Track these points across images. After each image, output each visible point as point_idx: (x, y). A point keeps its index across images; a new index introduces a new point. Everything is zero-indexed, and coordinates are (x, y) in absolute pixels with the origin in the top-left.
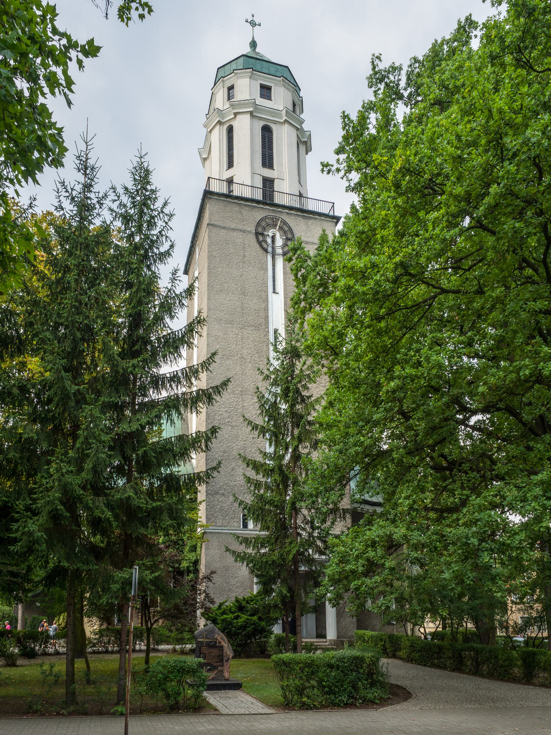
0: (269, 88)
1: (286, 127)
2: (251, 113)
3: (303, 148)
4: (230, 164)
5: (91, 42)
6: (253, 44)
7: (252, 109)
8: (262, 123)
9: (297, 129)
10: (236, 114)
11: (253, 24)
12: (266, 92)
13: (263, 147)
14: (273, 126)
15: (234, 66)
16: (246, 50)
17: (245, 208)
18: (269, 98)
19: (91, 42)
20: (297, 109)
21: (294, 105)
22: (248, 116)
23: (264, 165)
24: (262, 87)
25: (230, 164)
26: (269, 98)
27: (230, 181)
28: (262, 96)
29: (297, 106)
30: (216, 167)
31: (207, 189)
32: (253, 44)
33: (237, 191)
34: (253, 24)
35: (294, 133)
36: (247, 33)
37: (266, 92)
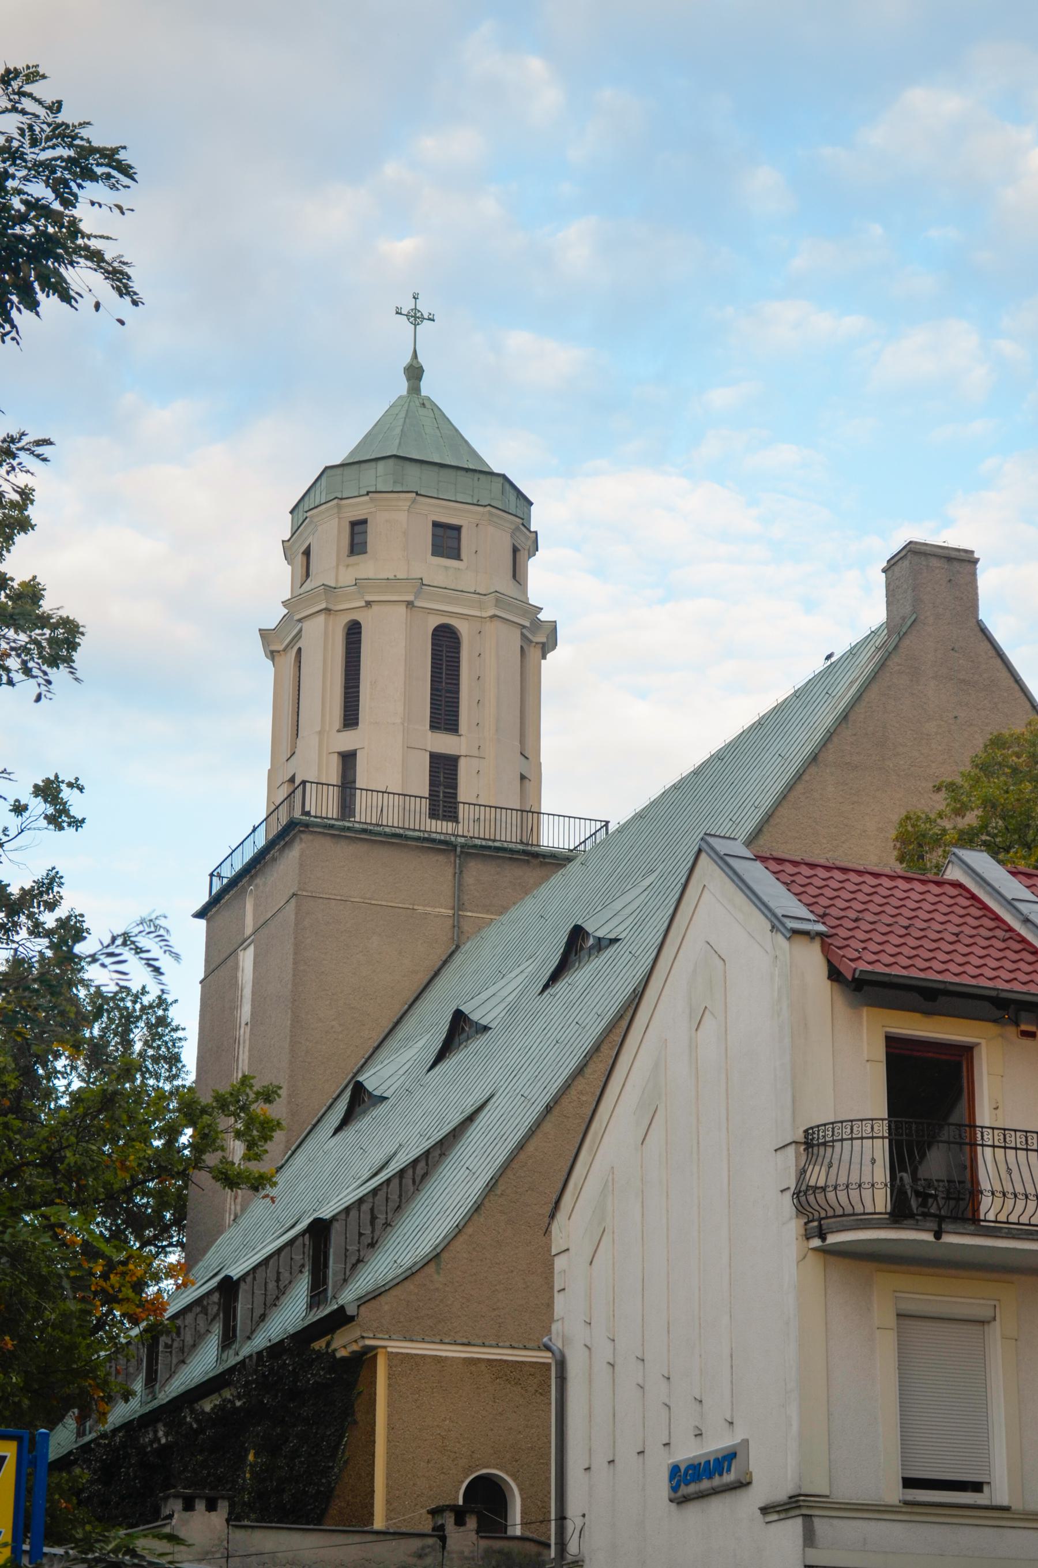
2: (410, 604)
4: (351, 718)
7: (410, 598)
8: (434, 621)
10: (369, 604)
12: (446, 540)
14: (463, 628)
22: (402, 609)
23: (435, 726)
25: (351, 718)
34: (416, 318)
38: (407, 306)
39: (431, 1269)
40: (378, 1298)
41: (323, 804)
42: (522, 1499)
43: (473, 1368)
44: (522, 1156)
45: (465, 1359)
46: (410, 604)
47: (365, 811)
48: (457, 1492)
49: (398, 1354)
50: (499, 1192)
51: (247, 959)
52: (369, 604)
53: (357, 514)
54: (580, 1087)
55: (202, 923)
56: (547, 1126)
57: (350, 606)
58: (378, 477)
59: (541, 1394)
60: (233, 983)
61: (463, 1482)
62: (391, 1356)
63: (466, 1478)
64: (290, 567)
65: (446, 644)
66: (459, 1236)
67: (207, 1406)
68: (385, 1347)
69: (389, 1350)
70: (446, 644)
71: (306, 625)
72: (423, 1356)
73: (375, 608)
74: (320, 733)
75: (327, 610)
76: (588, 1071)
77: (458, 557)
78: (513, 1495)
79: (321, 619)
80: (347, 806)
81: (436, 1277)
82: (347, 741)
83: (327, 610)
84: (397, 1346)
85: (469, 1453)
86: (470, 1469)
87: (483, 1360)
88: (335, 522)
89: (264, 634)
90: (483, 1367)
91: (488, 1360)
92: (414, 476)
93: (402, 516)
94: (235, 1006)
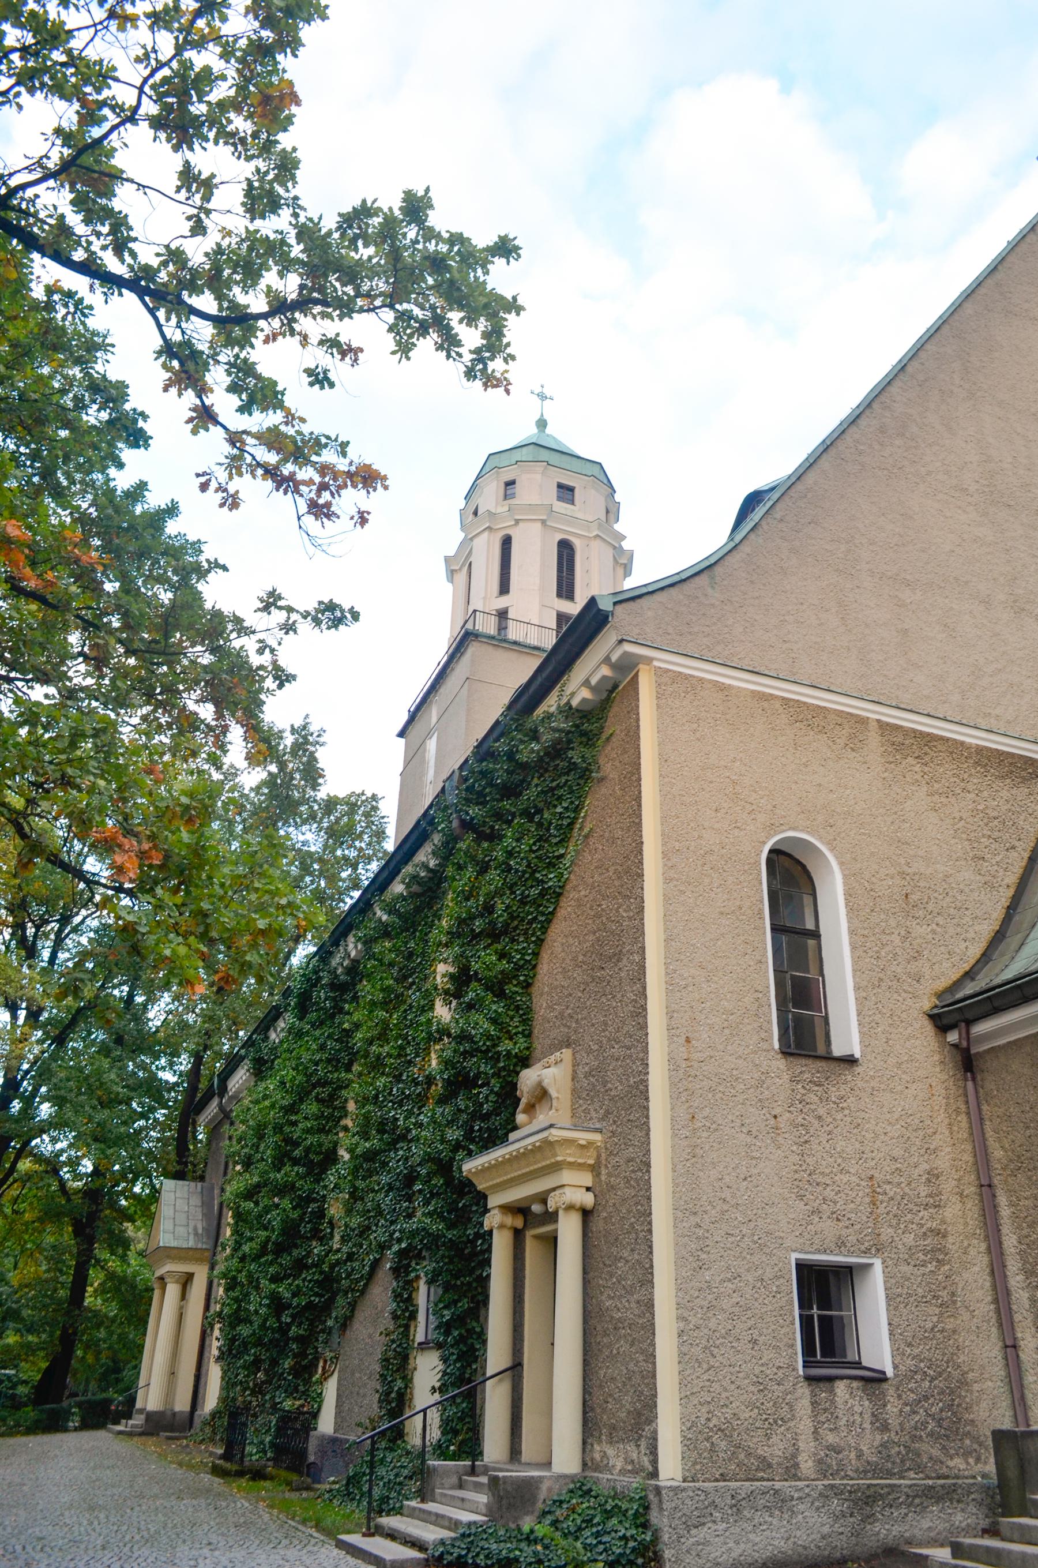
0: (571, 489)
1: (596, 544)
2: (543, 522)
3: (620, 571)
4: (504, 588)
5: (409, 197)
6: (542, 424)
7: (544, 517)
8: (559, 537)
9: (615, 548)
10: (517, 521)
11: (542, 397)
12: (566, 492)
13: (560, 570)
14: (577, 543)
15: (517, 455)
16: (528, 431)
17: (821, 1385)
18: (572, 502)
19: (409, 197)
20: (611, 516)
21: (607, 512)
22: (539, 525)
23: (559, 595)
24: (560, 486)
25: (504, 588)
26: (572, 502)
27: (502, 615)
28: (560, 498)
29: (612, 511)
30: (485, 596)
31: (469, 626)
32: (542, 424)
33: (514, 632)
34: (542, 397)
35: (610, 552)
36: (533, 410)
37: (566, 492)
38: (538, 390)
39: (703, 580)
40: (638, 601)
41: (487, 626)
42: (845, 876)
43: (765, 704)
44: (799, 487)
45: (753, 692)
46: (543, 522)
47: (514, 632)
48: (759, 855)
49: (668, 671)
50: (778, 516)
51: (432, 745)
52: (517, 521)
53: (509, 478)
54: (857, 436)
55: (402, 741)
56: (825, 463)
57: (504, 525)
58: (524, 454)
59: (853, 749)
60: (423, 761)
61: (764, 843)
62: (661, 672)
63: (768, 838)
64: (464, 502)
65: (566, 552)
66: (734, 553)
67: (398, 888)
68: (651, 659)
69: (656, 663)
70: (566, 552)
71: (476, 541)
72: (701, 680)
73: (521, 524)
74: (485, 598)
75: (489, 528)
76: (863, 422)
77: (573, 503)
78: (832, 872)
79: (486, 534)
80: (502, 628)
81: (710, 591)
82: (502, 602)
83: (489, 528)
84: (664, 660)
85: (770, 807)
86: (772, 828)
87: (777, 697)
88: (495, 483)
89: (447, 559)
90: (777, 704)
91: (784, 699)
92: (545, 455)
93: (538, 477)
94: (423, 774)
